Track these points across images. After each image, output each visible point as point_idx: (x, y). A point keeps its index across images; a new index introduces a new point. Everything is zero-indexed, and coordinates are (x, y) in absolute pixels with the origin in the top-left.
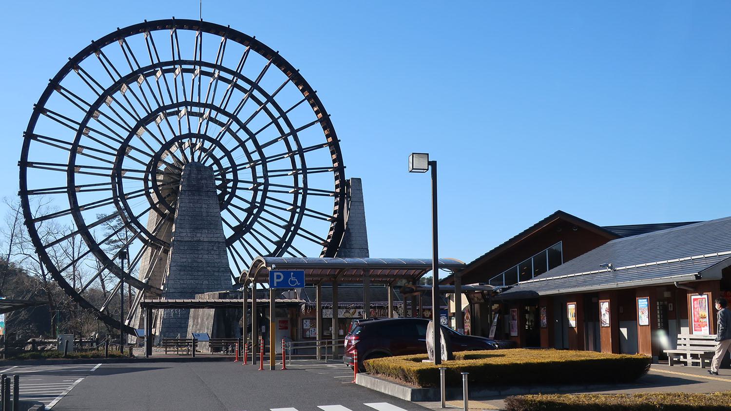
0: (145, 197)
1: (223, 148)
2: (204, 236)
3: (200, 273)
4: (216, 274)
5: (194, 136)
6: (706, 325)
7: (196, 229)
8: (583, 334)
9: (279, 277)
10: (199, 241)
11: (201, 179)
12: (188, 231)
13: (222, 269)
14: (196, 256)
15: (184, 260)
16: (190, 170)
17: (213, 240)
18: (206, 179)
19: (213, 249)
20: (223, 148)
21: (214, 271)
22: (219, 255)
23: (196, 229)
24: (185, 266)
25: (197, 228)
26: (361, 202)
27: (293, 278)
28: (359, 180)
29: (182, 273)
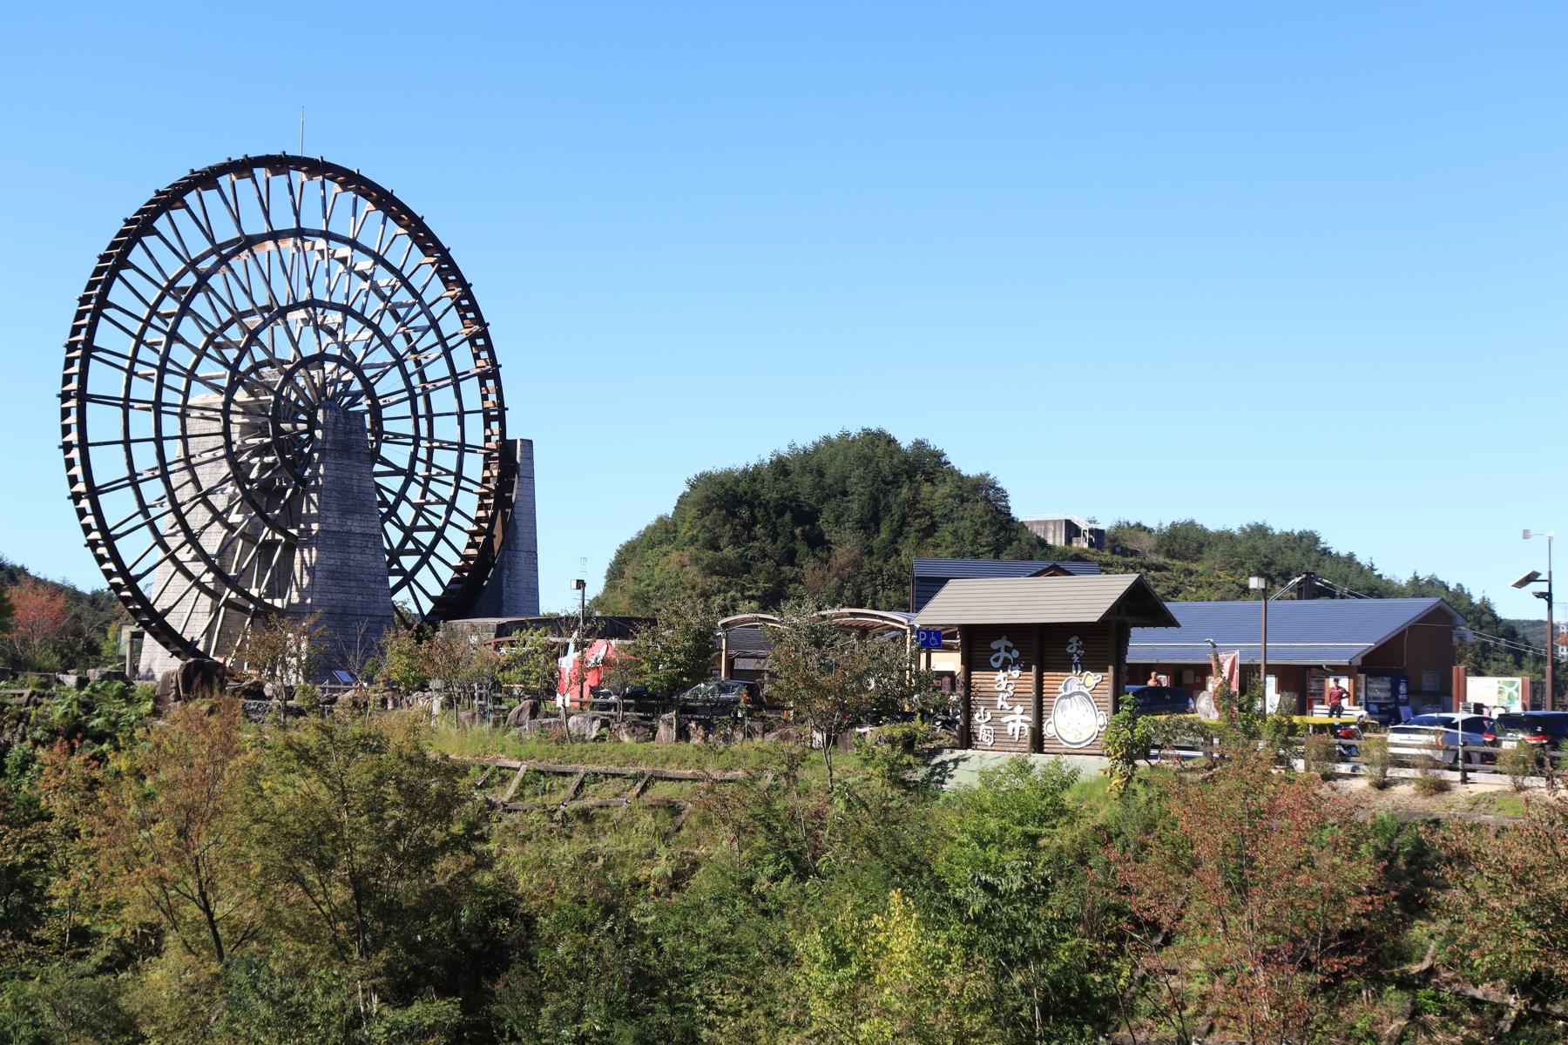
0: (130, 488)
1: (161, 454)
2: (355, 525)
3: (352, 584)
4: (372, 585)
5: (227, 404)
6: (1535, 706)
7: (345, 513)
8: (511, 616)
9: (923, 636)
10: (349, 532)
11: (351, 432)
12: (336, 516)
13: (379, 578)
14: (347, 556)
15: (332, 562)
16: (336, 417)
17: (368, 531)
18: (356, 432)
19: (367, 546)
20: (161, 454)
21: (370, 581)
22: (374, 555)
23: (345, 513)
24: (333, 572)
25: (349, 512)
26: (532, 478)
27: (933, 638)
28: (528, 444)
29: (330, 582)
